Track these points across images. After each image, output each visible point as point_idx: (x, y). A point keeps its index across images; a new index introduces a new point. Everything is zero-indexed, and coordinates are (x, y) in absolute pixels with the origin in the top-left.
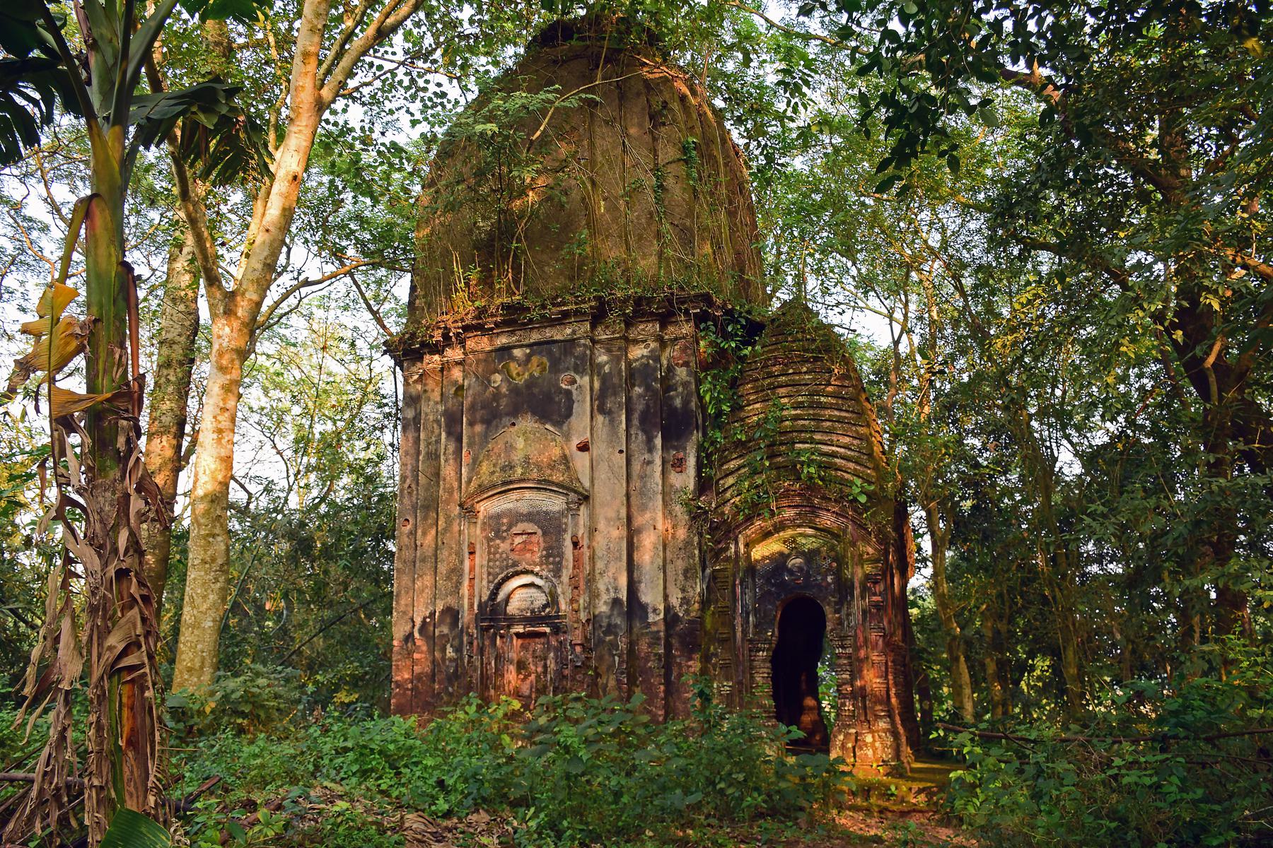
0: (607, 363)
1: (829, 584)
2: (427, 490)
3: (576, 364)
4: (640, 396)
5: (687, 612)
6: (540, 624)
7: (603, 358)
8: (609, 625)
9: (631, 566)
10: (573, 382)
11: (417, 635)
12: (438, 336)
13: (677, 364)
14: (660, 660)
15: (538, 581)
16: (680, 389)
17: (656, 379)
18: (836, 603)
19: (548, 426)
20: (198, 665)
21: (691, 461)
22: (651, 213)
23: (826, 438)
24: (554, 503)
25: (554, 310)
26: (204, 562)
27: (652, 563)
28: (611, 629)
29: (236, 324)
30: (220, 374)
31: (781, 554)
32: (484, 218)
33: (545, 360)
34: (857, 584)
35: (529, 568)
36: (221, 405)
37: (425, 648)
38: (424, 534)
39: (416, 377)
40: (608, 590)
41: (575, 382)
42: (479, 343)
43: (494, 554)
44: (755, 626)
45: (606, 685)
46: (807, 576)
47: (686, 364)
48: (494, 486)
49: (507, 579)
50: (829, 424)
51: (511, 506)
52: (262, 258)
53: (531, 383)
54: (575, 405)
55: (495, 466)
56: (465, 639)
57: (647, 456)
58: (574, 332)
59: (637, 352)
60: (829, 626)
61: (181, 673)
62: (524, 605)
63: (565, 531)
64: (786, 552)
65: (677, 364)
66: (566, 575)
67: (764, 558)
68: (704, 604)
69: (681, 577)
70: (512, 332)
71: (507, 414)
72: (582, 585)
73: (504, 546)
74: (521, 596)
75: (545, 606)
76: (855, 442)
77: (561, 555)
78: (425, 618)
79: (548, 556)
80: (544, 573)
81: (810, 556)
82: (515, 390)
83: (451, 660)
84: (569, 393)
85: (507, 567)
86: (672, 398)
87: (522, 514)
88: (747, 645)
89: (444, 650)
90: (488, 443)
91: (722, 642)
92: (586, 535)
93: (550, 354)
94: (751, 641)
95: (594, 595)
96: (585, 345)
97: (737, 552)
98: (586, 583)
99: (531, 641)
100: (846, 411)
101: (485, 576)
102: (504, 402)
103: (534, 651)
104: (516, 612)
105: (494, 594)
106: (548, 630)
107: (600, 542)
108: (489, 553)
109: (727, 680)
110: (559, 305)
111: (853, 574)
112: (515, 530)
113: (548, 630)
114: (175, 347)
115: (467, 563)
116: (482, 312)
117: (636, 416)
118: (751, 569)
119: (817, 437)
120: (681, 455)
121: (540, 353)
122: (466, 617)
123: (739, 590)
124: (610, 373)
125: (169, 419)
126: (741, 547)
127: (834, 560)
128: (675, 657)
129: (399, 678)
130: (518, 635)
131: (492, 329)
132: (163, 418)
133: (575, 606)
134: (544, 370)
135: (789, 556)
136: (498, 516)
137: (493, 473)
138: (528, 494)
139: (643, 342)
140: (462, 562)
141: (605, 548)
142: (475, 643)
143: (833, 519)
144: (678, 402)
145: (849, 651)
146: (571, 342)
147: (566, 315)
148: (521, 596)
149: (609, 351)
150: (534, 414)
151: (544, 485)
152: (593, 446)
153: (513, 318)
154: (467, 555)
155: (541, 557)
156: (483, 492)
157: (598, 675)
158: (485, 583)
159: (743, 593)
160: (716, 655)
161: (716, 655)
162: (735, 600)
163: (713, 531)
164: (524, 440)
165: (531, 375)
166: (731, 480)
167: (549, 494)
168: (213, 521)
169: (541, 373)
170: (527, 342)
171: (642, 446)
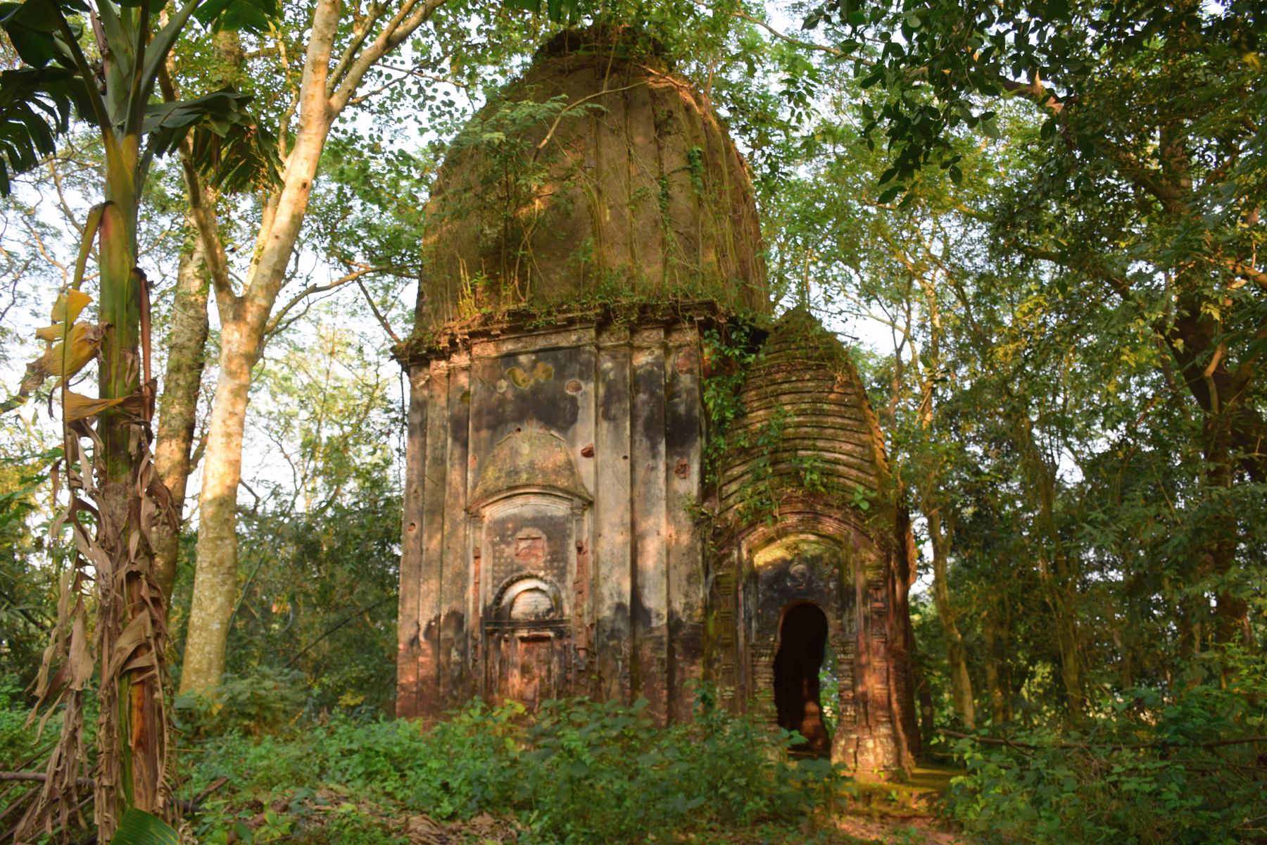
1: (831, 591)
2: (433, 494)
5: (690, 617)
6: (543, 629)
7: (608, 365)
8: (613, 630)
9: (635, 572)
10: (578, 388)
12: (444, 343)
18: (838, 609)
19: (553, 432)
20: (205, 667)
21: (695, 468)
22: (656, 222)
23: (828, 445)
24: (558, 509)
25: (561, 317)
26: (212, 565)
28: (614, 634)
29: (245, 329)
30: (229, 379)
31: (784, 560)
33: (550, 366)
34: (859, 590)
36: (230, 409)
37: (429, 652)
38: (430, 538)
40: (611, 595)
44: (758, 632)
46: (810, 582)
47: (690, 371)
48: (500, 491)
49: (511, 583)
50: (831, 431)
51: (516, 511)
52: (271, 264)
53: (536, 390)
54: (580, 412)
55: (500, 471)
57: (651, 462)
58: (579, 339)
60: (831, 632)
61: (189, 674)
62: (528, 609)
63: (569, 536)
66: (570, 580)
67: (767, 564)
68: (708, 609)
69: (684, 583)
70: (518, 338)
71: (514, 420)
72: (586, 590)
73: (509, 551)
74: (526, 600)
75: (549, 611)
77: (565, 560)
78: (430, 622)
79: (552, 561)
80: (549, 578)
81: (813, 562)
82: (521, 397)
84: (573, 400)
85: (512, 572)
86: (676, 405)
87: (527, 520)
91: (726, 647)
92: (590, 541)
93: (555, 360)
94: (753, 646)
97: (740, 558)
98: (590, 587)
100: (850, 418)
101: (490, 581)
102: (509, 408)
104: (520, 616)
105: (499, 598)
106: (551, 634)
107: (605, 546)
108: (494, 557)
110: (565, 312)
111: (855, 581)
112: (520, 535)
113: (551, 634)
114: (184, 351)
115: (472, 568)
116: (488, 319)
117: (640, 422)
118: (754, 575)
119: (820, 444)
120: (685, 461)
121: (546, 359)
122: (471, 621)
123: (741, 596)
124: (615, 380)
125: (178, 423)
126: (744, 553)
128: (678, 662)
130: (523, 639)
131: (498, 336)
132: (173, 422)
133: (579, 611)
134: (549, 376)
136: (502, 522)
138: (533, 500)
139: (648, 348)
140: (467, 566)
142: (480, 647)
143: (835, 526)
144: (682, 409)
146: (576, 349)
147: (571, 322)
148: (526, 600)
149: (614, 358)
150: (540, 419)
151: (548, 491)
152: (597, 453)
153: (519, 324)
154: (472, 559)
157: (601, 679)
158: (489, 587)
159: (746, 599)
160: (718, 660)
161: (718, 660)
162: (737, 605)
163: (715, 538)
164: (530, 446)
165: (537, 382)
166: (734, 487)
167: (553, 499)
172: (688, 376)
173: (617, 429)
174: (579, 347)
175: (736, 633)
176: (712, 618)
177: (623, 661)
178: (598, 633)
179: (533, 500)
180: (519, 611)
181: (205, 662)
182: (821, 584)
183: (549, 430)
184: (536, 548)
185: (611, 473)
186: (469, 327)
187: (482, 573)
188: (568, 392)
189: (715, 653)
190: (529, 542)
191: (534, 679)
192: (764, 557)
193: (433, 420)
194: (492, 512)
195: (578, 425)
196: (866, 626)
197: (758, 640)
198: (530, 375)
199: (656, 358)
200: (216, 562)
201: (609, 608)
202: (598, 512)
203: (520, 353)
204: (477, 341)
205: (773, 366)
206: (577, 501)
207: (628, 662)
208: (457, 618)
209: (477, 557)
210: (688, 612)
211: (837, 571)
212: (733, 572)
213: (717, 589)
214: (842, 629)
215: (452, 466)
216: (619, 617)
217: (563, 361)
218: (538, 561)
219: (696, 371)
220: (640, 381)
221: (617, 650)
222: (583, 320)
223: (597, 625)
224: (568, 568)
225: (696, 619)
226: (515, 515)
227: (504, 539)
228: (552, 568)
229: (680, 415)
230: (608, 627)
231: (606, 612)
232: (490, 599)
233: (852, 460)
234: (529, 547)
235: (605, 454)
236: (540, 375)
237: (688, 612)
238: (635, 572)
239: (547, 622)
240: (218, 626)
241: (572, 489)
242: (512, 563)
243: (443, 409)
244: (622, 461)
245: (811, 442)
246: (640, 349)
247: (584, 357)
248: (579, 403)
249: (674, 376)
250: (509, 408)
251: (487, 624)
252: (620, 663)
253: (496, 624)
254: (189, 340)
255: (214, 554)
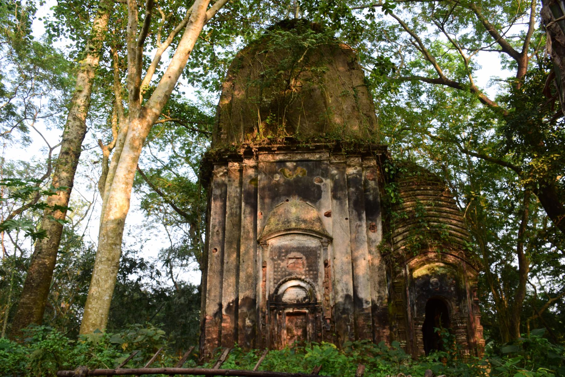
0: (337, 174)
1: (452, 291)
5: (381, 303)
6: (302, 308)
7: (335, 172)
8: (344, 309)
9: (354, 278)
10: (321, 181)
11: (224, 313)
12: (242, 152)
14: (370, 328)
15: (302, 284)
16: (372, 191)
18: (457, 301)
19: (308, 203)
20: (99, 323)
21: (380, 227)
22: (353, 107)
24: (312, 243)
25: (313, 144)
26: (108, 260)
28: (345, 311)
29: (145, 124)
30: (131, 152)
31: (427, 275)
32: (266, 97)
33: (305, 169)
34: (468, 291)
35: (299, 276)
36: (129, 168)
37: (229, 320)
38: (229, 256)
39: (221, 173)
40: (342, 290)
42: (266, 158)
43: (277, 268)
44: (417, 312)
45: (343, 342)
48: (279, 231)
49: (285, 282)
50: (445, 214)
51: (287, 243)
52: (164, 91)
53: (297, 180)
54: (323, 193)
56: (260, 314)
57: (358, 223)
58: (320, 157)
59: (351, 171)
60: (454, 312)
61: (88, 327)
63: (319, 257)
64: (430, 275)
66: (320, 281)
67: (419, 277)
68: (389, 299)
69: (377, 286)
70: (286, 154)
71: (284, 195)
72: (330, 286)
73: (283, 264)
74: (292, 292)
75: (305, 298)
76: (459, 223)
77: (317, 270)
78: (229, 303)
79: (309, 271)
80: (308, 280)
81: (441, 277)
82: (288, 183)
83: (248, 327)
84: (319, 187)
85: (285, 276)
86: (368, 195)
87: (293, 248)
88: (414, 322)
89: (244, 321)
90: (273, 209)
91: (399, 320)
92: (331, 260)
93: (307, 166)
94: (415, 319)
95: (336, 293)
96: (327, 164)
97: (406, 273)
98: (330, 285)
99: (294, 317)
100: (453, 209)
101: (272, 280)
102: (281, 189)
103: (296, 323)
104: (288, 301)
105: (277, 290)
106: (307, 311)
107: (338, 262)
108: (274, 267)
109: (403, 340)
110: (315, 142)
111: (465, 286)
112: (290, 256)
113: (307, 311)
114: (72, 144)
115: (261, 273)
116: (271, 141)
117: (352, 202)
118: (413, 281)
119: (441, 219)
120: (374, 224)
121: (302, 165)
122: (260, 301)
123: (408, 293)
124: (339, 179)
125: (65, 183)
126: (408, 271)
127: (454, 280)
129: (210, 338)
130: (289, 314)
131: (275, 151)
132: (62, 182)
134: (304, 174)
135: (431, 277)
136: (280, 248)
137: (278, 224)
139: (354, 166)
140: (258, 272)
141: (340, 268)
142: (267, 317)
143: (453, 259)
144: (371, 197)
145: (465, 325)
146: (319, 162)
148: (292, 292)
149: (337, 169)
150: (299, 195)
151: (308, 232)
152: (332, 215)
153: (291, 146)
154: (261, 268)
155: (306, 271)
156: (272, 234)
157: (338, 336)
158: (272, 284)
159: (410, 294)
160: (395, 327)
161: (395, 327)
163: (391, 262)
164: (295, 209)
165: (297, 176)
166: (400, 238)
167: (309, 237)
169: (303, 175)
171: (355, 217)
172: (373, 182)
173: (341, 204)
175: (407, 312)
178: (336, 311)
179: (297, 237)
180: (286, 298)
181: (99, 319)
182: (447, 288)
184: (298, 263)
185: (339, 226)
186: (260, 144)
187: (268, 276)
188: (316, 183)
189: (393, 323)
190: (294, 260)
191: (294, 336)
192: (419, 272)
194: (274, 242)
195: (322, 200)
196: (472, 309)
197: (418, 315)
198: (292, 171)
199: (358, 171)
200: (111, 258)
201: (341, 297)
202: (335, 246)
203: (287, 161)
204: (262, 153)
206: (324, 239)
208: (251, 302)
209: (264, 267)
210: (380, 301)
211: (454, 282)
212: (402, 281)
213: (393, 288)
214: (460, 311)
216: (347, 302)
217: (312, 167)
218: (301, 270)
219: (377, 180)
220: (353, 181)
221: (347, 320)
222: (326, 147)
223: (336, 305)
224: (319, 275)
225: (385, 305)
226: (286, 245)
227: (279, 257)
228: (309, 275)
229: (370, 201)
230: (341, 307)
231: (340, 299)
232: (272, 290)
233: (457, 228)
234: (294, 263)
235: (336, 216)
236: (299, 172)
237: (380, 301)
238: (354, 278)
240: (108, 298)
241: (322, 232)
242: (285, 271)
244: (345, 220)
245: (436, 219)
246: (349, 166)
247: (324, 166)
248: (322, 189)
249: (366, 181)
250: (281, 189)
251: (271, 304)
252: (349, 327)
254: (75, 138)
255: (110, 253)
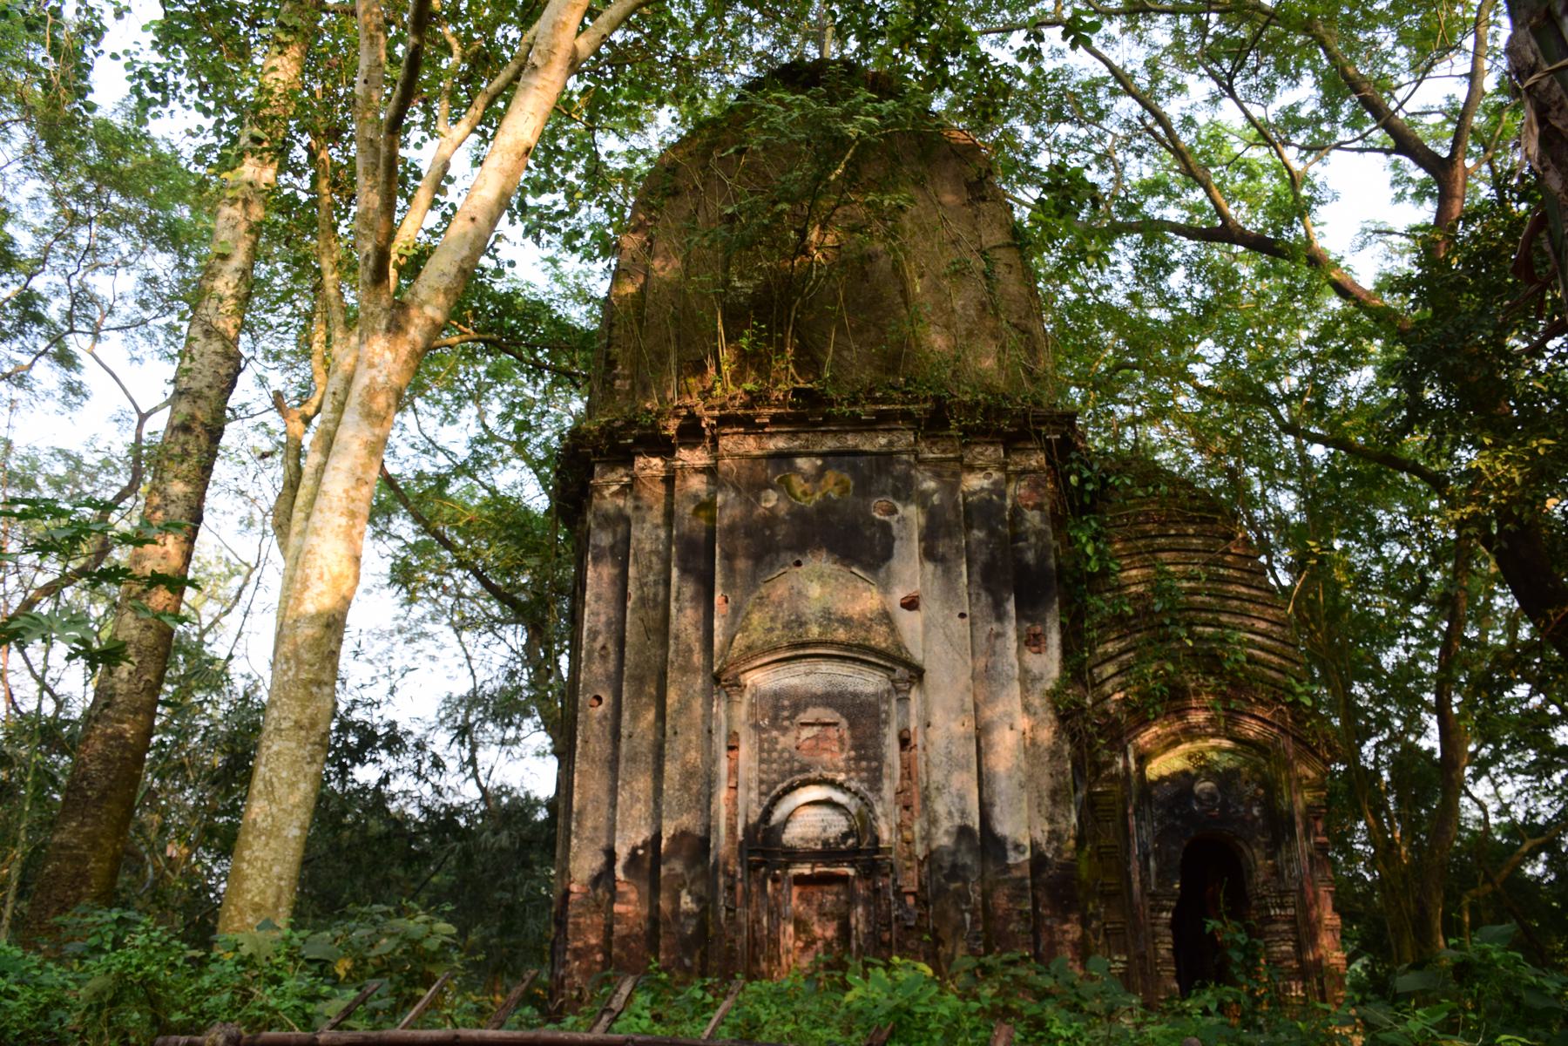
0: (935, 491)
1: (1256, 818)
2: (639, 652)
3: (895, 486)
4: (980, 542)
5: (1058, 851)
6: (838, 863)
7: (930, 485)
8: (954, 866)
9: (984, 780)
10: (893, 511)
12: (672, 427)
13: (1027, 506)
14: (1027, 920)
15: (839, 797)
16: (1033, 540)
17: (1003, 522)
18: (1267, 845)
19: (855, 570)
20: (271, 900)
21: (1054, 638)
22: (983, 304)
23: (1236, 620)
24: (867, 682)
26: (298, 725)
27: (1010, 777)
28: (956, 872)
29: (404, 350)
30: (364, 425)
31: (1185, 773)
32: (742, 277)
33: (846, 477)
34: (1298, 819)
35: (830, 775)
36: (359, 472)
37: (633, 896)
38: (635, 718)
39: (615, 488)
40: (950, 813)
41: (895, 511)
43: (769, 752)
44: (1158, 875)
45: (953, 957)
46: (1225, 806)
47: (1038, 507)
48: (776, 649)
49: (791, 789)
50: (1236, 603)
51: (795, 681)
52: (458, 258)
53: (826, 508)
54: (897, 544)
55: (773, 619)
56: (721, 880)
57: (995, 626)
58: (891, 443)
59: (974, 482)
61: (241, 912)
62: (812, 832)
63: (886, 722)
64: (1194, 772)
65: (1027, 506)
66: (888, 789)
67: (1162, 779)
68: (1080, 840)
69: (1047, 801)
72: (917, 804)
73: (786, 741)
74: (809, 819)
75: (845, 836)
77: (880, 758)
78: (634, 849)
79: (858, 759)
80: (854, 785)
81: (1226, 779)
82: (799, 515)
83: (688, 915)
84: (885, 527)
85: (791, 773)
86: (1021, 551)
87: (814, 695)
88: (1149, 902)
90: (757, 587)
91: (1106, 897)
92: (919, 731)
93: (854, 470)
94: (1153, 896)
95: (933, 821)
96: (908, 462)
97: (1126, 767)
98: (915, 798)
99: (814, 889)
100: (1257, 588)
101: (754, 785)
102: (782, 532)
103: (821, 905)
104: (798, 844)
105: (767, 813)
106: (851, 872)
107: (938, 736)
108: (761, 750)
110: (876, 401)
111: (1291, 804)
112: (804, 717)
113: (851, 872)
114: (200, 402)
115: (723, 766)
116: (755, 399)
117: (976, 569)
119: (1224, 618)
120: (1038, 629)
121: (839, 467)
122: (722, 844)
123: (1133, 822)
124: (941, 506)
125: (180, 511)
126: (1132, 761)
128: (1043, 917)
130: (800, 880)
131: (765, 425)
132: (172, 508)
134: (846, 490)
135: (1196, 778)
136: (777, 696)
137: (771, 630)
138: (825, 667)
139: (982, 469)
140: (715, 761)
142: (739, 887)
144: (1030, 556)
145: (1291, 911)
146: (886, 458)
147: (883, 417)
148: (809, 819)
149: (937, 476)
150: (832, 550)
151: (856, 653)
152: (920, 603)
153: (808, 413)
154: (723, 751)
155: (848, 759)
157: (938, 941)
158: (754, 795)
159: (1139, 827)
160: (1097, 916)
162: (1127, 835)
163: (1086, 737)
164: (818, 587)
165: (826, 496)
166: (1110, 669)
167: (858, 667)
168: (323, 660)
169: (841, 494)
170: (817, 449)
171: (987, 611)
172: (1036, 513)
173: (948, 574)
174: (891, 454)
175: (1128, 876)
176: (1085, 854)
177: (972, 913)
178: (931, 871)
180: (794, 834)
181: (271, 892)
182: (1242, 809)
183: (848, 566)
186: (723, 407)
187: (742, 772)
190: (816, 729)
192: (1165, 765)
193: (639, 541)
194: (761, 679)
197: (1159, 885)
198: (811, 483)
199: (995, 483)
200: (306, 722)
201: (947, 832)
204: (727, 430)
205: (1139, 514)
206: (901, 672)
207: (980, 913)
208: (697, 846)
209: (731, 748)
211: (1261, 791)
212: (1117, 788)
213: (1091, 810)
214: (1276, 872)
215: (680, 610)
216: (963, 847)
218: (835, 757)
219: (1047, 508)
223: (932, 857)
225: (1067, 855)
226: (795, 687)
228: (858, 770)
229: (1027, 565)
230: (947, 862)
231: (943, 840)
233: (1268, 642)
234: (816, 737)
235: (932, 606)
236: (831, 485)
238: (984, 780)
239: (843, 852)
240: (297, 832)
241: (893, 651)
242: (791, 759)
243: (657, 527)
244: (959, 620)
246: (971, 469)
247: (900, 468)
248: (895, 532)
249: (1017, 512)
251: (751, 852)
252: (968, 916)
253: (763, 853)
254: (209, 387)
255: (304, 707)
